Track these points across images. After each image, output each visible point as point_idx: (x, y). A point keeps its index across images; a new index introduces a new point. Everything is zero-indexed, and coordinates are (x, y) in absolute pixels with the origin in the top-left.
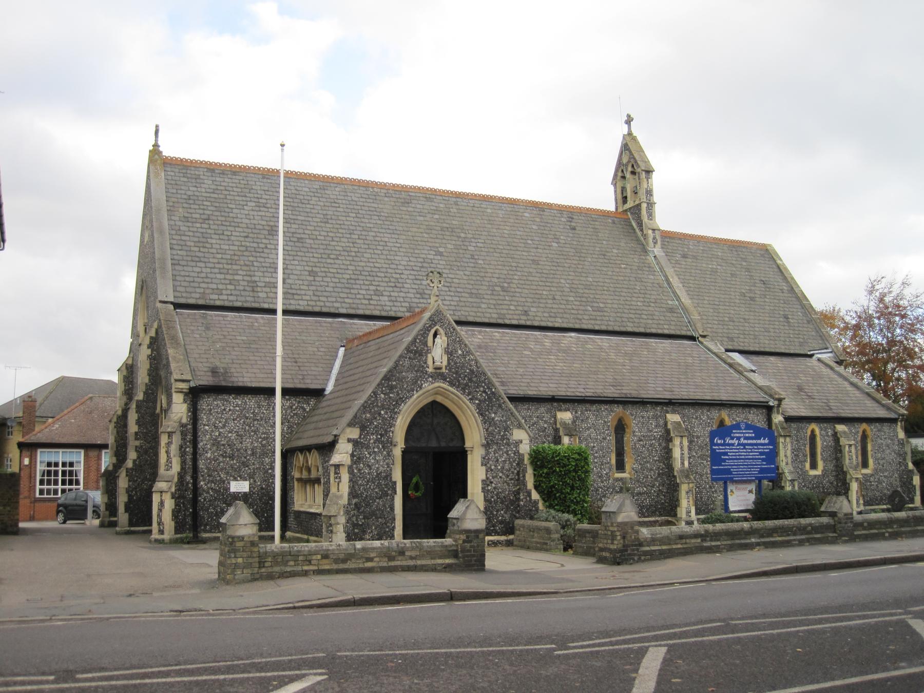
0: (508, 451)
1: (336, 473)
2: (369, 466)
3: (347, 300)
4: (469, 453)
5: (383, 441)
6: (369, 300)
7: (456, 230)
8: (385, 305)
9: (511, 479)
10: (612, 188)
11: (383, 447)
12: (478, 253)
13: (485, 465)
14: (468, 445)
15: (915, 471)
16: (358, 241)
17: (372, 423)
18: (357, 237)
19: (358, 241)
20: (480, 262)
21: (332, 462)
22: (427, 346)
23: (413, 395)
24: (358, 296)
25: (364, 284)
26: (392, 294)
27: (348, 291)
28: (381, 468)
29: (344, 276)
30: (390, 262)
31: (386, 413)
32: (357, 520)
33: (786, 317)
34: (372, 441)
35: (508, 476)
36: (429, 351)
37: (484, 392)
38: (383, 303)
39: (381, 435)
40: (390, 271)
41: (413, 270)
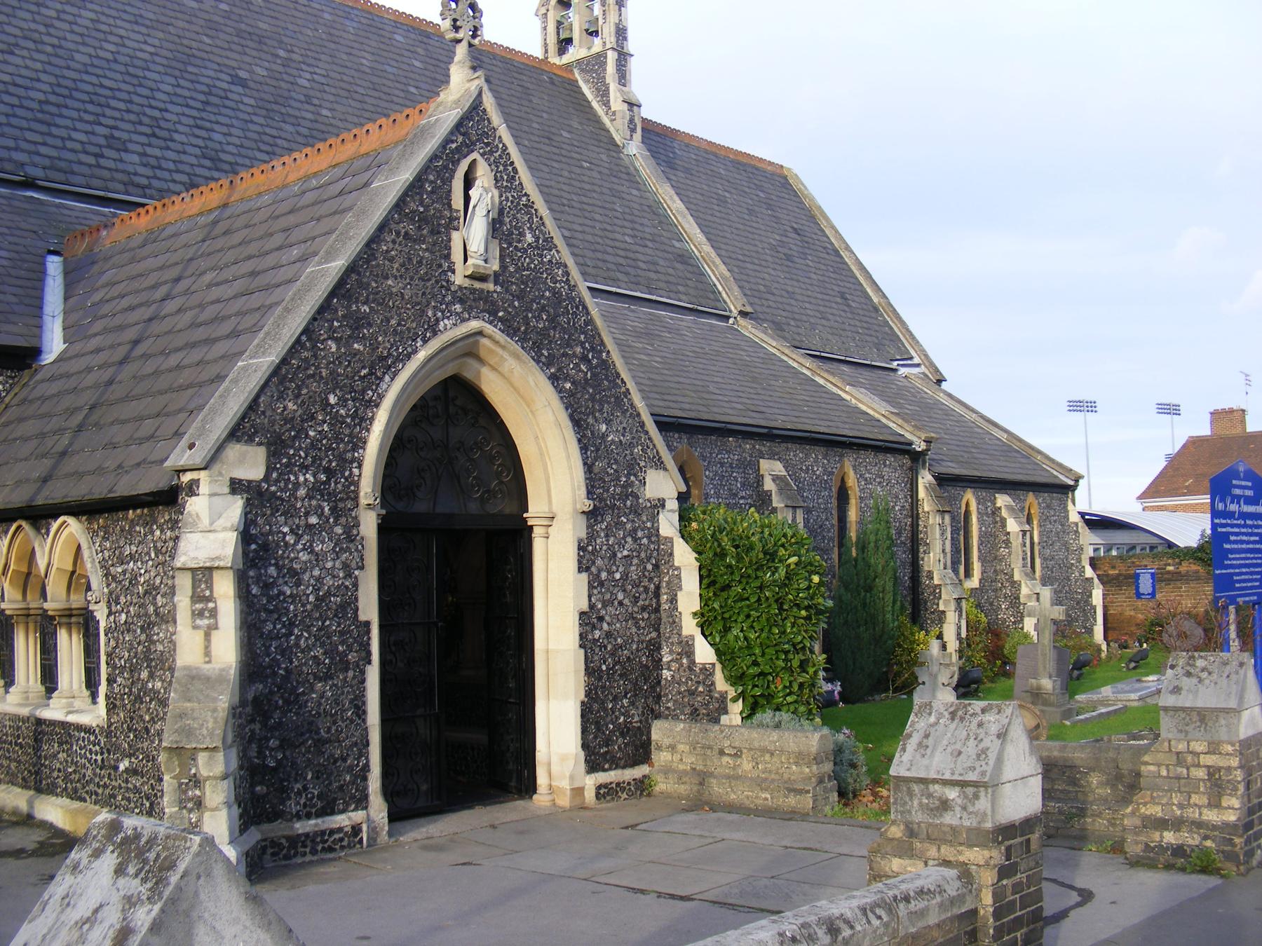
0: (635, 530)
1: (197, 598)
2: (294, 573)
3: (43, 150)
4: (537, 532)
5: (334, 494)
6: (96, 155)
7: (267, 41)
8: (136, 174)
9: (644, 609)
10: (537, 23)
11: (333, 510)
12: (318, 95)
13: (588, 569)
14: (536, 509)
15: (1096, 581)
16: (57, 24)
17: (302, 432)
18: (53, 14)
19: (57, 24)
20: (325, 112)
21: (180, 561)
22: (450, 205)
23: (415, 351)
24: (69, 144)
25: (81, 120)
26: (149, 150)
27: (44, 129)
28: (329, 581)
29: (32, 94)
30: (135, 81)
31: (342, 401)
32: (260, 753)
33: (843, 296)
34: (302, 492)
35: (636, 600)
36: (452, 224)
37: (584, 358)
38: (131, 169)
39: (329, 472)
40: (136, 99)
41: (187, 106)
